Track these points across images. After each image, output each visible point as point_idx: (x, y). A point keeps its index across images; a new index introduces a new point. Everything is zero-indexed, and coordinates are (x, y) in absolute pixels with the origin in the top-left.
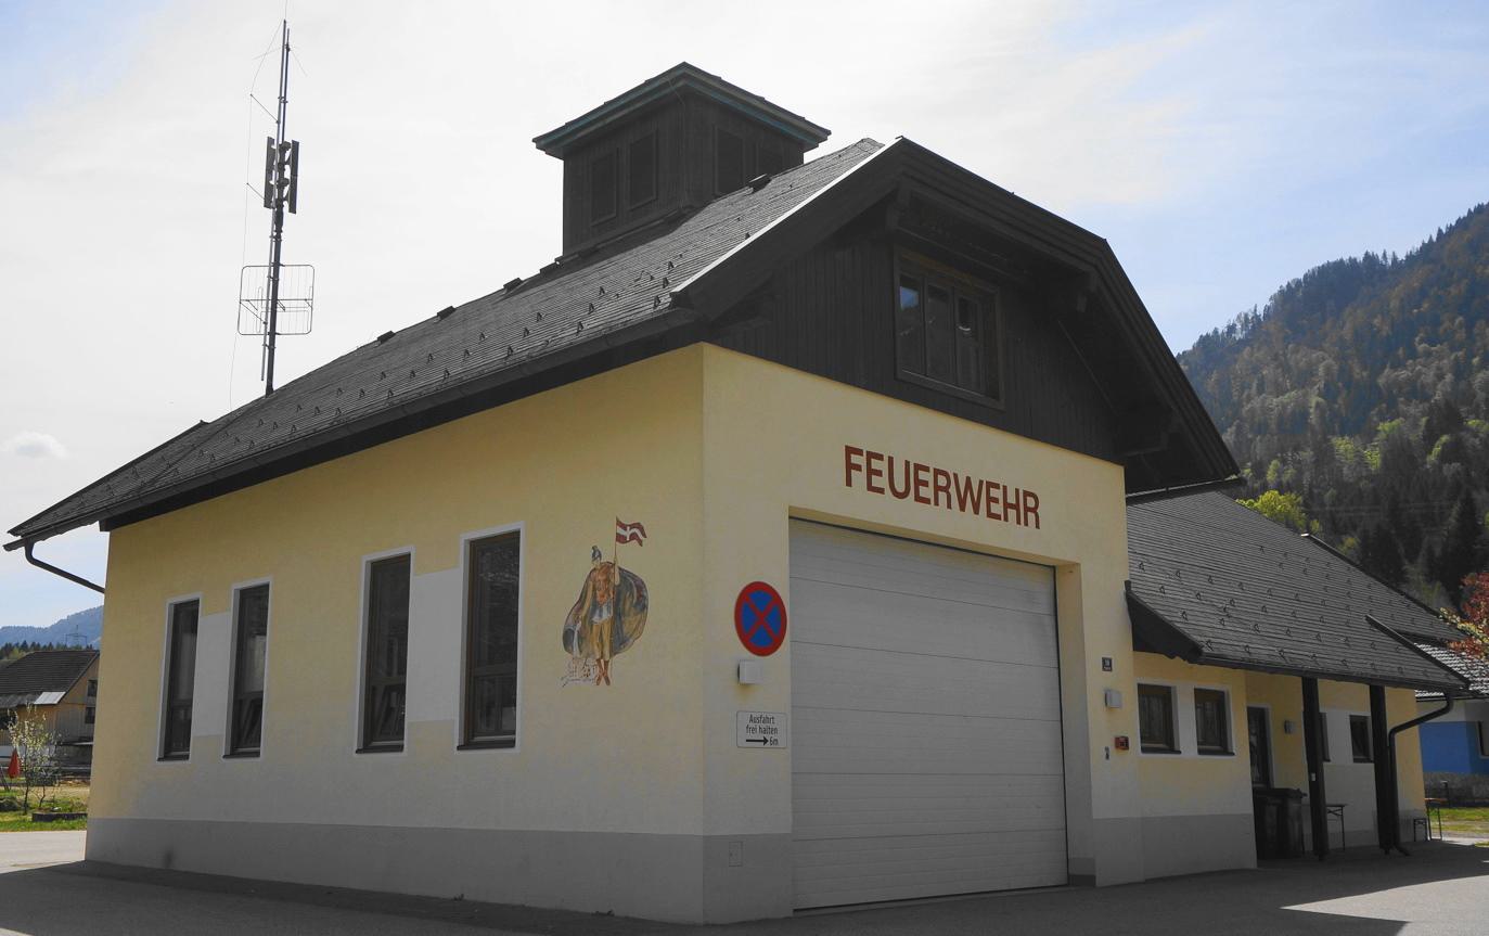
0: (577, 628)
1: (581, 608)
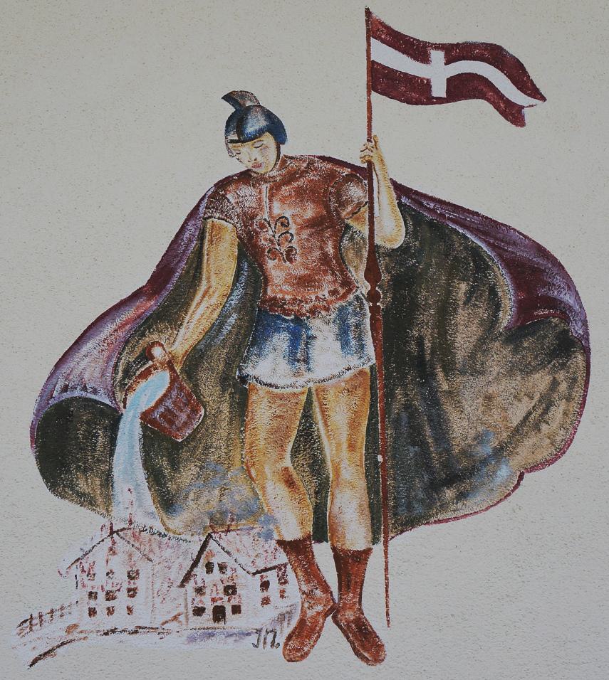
0: (150, 391)
1: (171, 314)
